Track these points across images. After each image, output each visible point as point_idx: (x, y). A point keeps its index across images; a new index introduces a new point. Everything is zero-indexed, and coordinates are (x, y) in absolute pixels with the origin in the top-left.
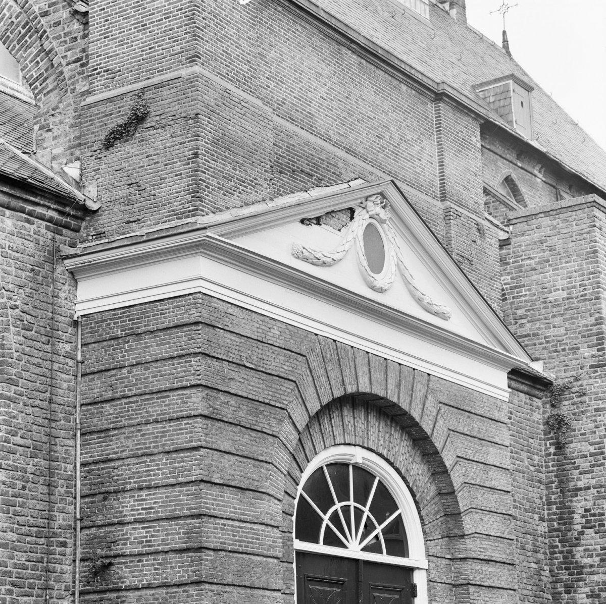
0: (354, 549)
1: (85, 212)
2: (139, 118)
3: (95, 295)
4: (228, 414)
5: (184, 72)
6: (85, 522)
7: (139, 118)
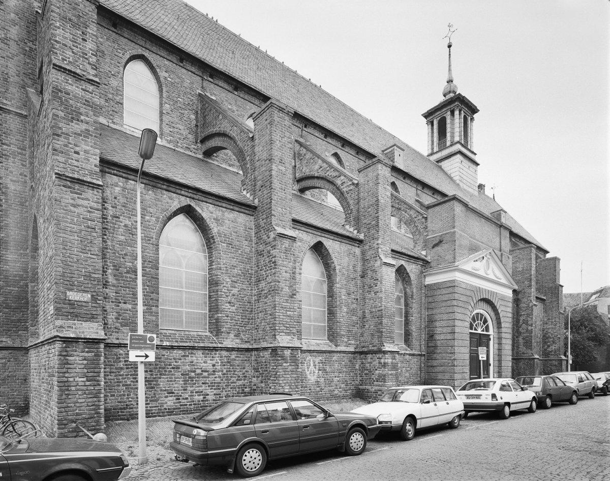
0: (479, 331)
1: (255, 208)
2: (441, 242)
3: (429, 280)
4: (460, 305)
5: (452, 231)
6: (428, 326)
7: (441, 242)
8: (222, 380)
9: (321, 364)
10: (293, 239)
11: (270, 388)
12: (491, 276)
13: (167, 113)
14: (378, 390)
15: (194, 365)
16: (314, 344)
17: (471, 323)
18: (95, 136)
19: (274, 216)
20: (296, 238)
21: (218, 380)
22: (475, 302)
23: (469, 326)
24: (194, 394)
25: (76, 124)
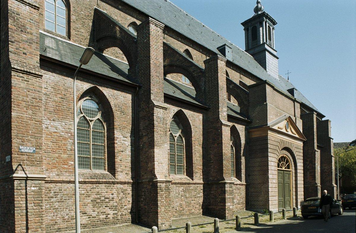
8: (118, 204)
9: (183, 192)
10: (165, 109)
11: (151, 208)
12: (290, 133)
13: (73, 21)
14: (221, 209)
15: (99, 194)
16: (178, 178)
17: (278, 163)
18: (37, 43)
19: (152, 94)
20: (167, 108)
21: (115, 204)
22: (280, 149)
23: (277, 166)
24: (100, 214)
25: (24, 34)
